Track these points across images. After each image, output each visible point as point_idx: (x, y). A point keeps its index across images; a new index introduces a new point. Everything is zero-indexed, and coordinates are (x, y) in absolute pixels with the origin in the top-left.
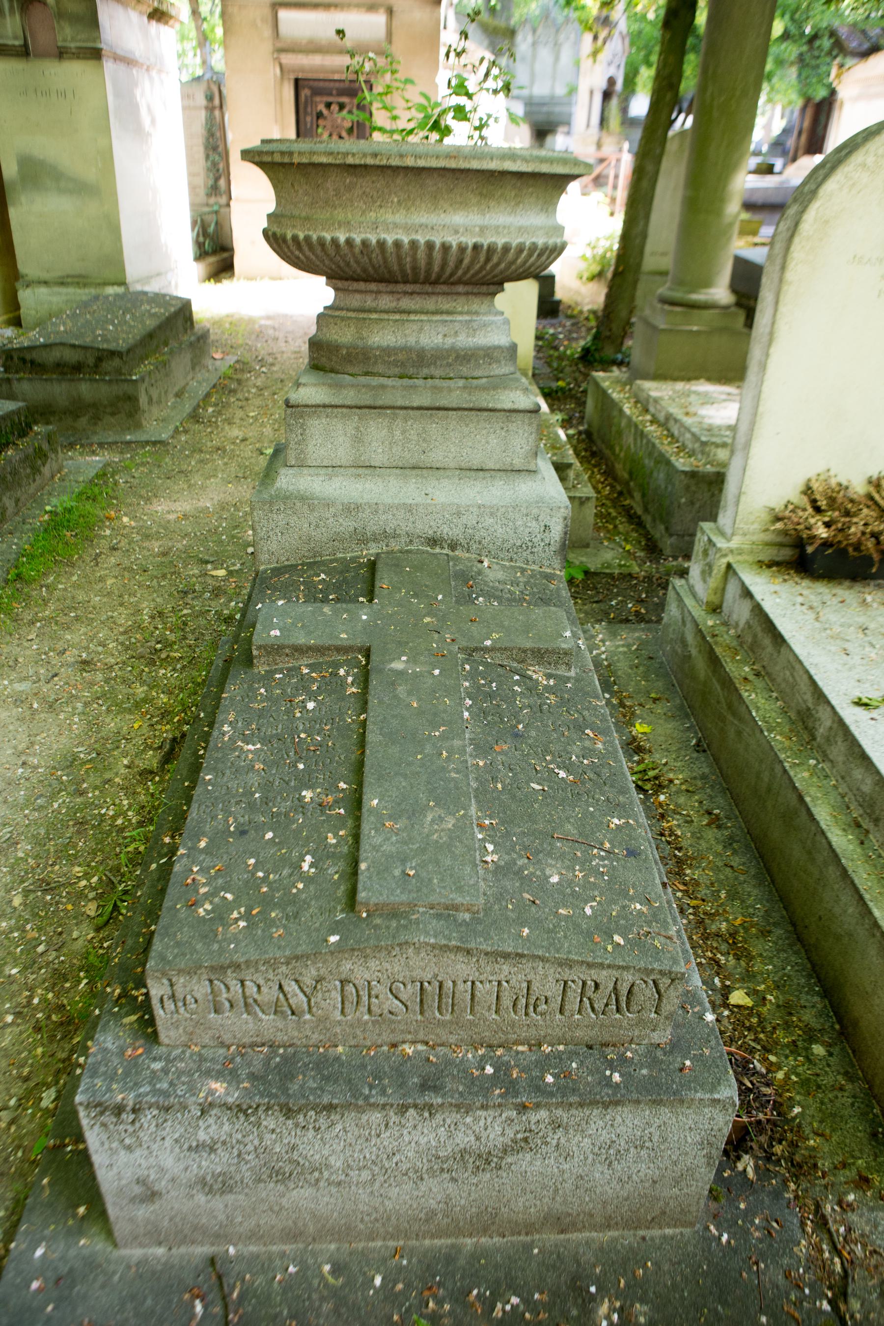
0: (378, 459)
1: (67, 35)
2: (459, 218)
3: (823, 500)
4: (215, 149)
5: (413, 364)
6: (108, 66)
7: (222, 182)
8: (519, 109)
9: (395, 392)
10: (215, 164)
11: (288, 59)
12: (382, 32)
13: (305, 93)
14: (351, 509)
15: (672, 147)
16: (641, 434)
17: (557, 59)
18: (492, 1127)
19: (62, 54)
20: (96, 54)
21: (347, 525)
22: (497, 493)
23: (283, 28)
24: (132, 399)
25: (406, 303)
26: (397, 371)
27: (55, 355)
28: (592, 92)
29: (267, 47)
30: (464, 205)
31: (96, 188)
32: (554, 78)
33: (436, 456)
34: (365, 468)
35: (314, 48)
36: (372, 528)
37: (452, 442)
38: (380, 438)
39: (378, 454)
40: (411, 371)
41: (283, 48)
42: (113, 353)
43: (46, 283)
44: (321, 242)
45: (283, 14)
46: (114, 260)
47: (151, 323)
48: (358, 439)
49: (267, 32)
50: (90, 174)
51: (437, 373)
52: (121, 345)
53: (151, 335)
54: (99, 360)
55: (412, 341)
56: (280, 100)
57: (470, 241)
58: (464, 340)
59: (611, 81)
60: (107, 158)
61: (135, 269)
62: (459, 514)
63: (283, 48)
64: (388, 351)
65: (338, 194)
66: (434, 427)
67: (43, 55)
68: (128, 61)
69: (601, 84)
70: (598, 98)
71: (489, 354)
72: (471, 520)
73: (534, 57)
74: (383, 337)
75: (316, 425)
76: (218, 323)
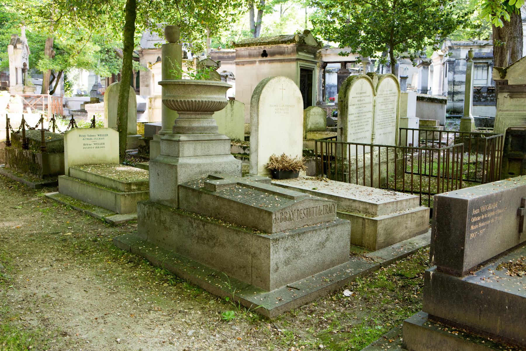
0: (199, 154)
2: (209, 96)
14: (199, 165)
16: (10, 221)
18: (323, 235)
21: (198, 170)
25: (198, 116)
26: (199, 132)
28: (16, 69)
30: (215, 93)
33: (211, 152)
36: (203, 170)
40: (203, 132)
44: (188, 101)
51: (208, 132)
55: (201, 125)
57: (218, 101)
59: (25, 65)
62: (221, 165)
64: (197, 127)
65: (191, 91)
66: (210, 144)
69: (21, 66)
70: (20, 72)
72: (223, 166)
74: (195, 124)
75: (186, 146)
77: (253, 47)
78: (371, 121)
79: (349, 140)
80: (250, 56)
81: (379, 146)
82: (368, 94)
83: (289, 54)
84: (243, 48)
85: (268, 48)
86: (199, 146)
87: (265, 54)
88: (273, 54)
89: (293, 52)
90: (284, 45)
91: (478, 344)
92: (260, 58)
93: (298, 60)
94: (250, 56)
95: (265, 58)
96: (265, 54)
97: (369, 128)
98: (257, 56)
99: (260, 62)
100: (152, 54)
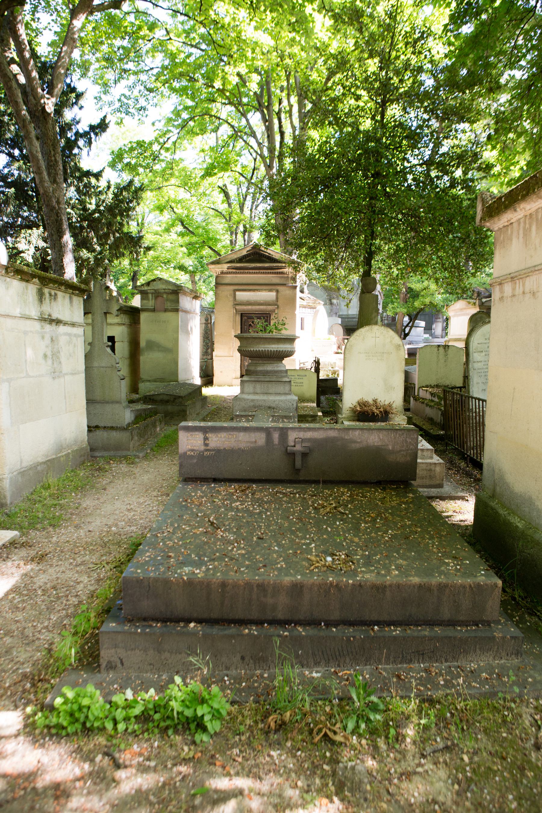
1: (169, 305)
2: (273, 346)
3: (363, 404)
4: (207, 338)
5: (266, 373)
6: (180, 313)
8: (339, 321)
9: (262, 378)
10: (207, 344)
11: (238, 307)
12: (274, 298)
13: (245, 318)
14: (253, 400)
19: (166, 310)
20: (177, 310)
21: (252, 404)
23: (237, 298)
24: (184, 411)
27: (161, 397)
29: (231, 303)
31: (172, 351)
33: (270, 391)
34: (255, 393)
35: (249, 303)
37: (273, 388)
38: (259, 387)
39: (258, 391)
41: (237, 303)
42: (180, 397)
43: (149, 381)
45: (238, 293)
46: (175, 373)
47: (190, 391)
48: (254, 388)
49: (232, 299)
50: (170, 345)
52: (182, 394)
53: (190, 394)
56: (235, 321)
58: (276, 369)
60: (176, 341)
61: (181, 377)
63: (237, 303)
66: (270, 385)
67: (160, 311)
68: (186, 312)
71: (281, 371)
74: (260, 368)
76: (210, 397)
86: (258, 386)
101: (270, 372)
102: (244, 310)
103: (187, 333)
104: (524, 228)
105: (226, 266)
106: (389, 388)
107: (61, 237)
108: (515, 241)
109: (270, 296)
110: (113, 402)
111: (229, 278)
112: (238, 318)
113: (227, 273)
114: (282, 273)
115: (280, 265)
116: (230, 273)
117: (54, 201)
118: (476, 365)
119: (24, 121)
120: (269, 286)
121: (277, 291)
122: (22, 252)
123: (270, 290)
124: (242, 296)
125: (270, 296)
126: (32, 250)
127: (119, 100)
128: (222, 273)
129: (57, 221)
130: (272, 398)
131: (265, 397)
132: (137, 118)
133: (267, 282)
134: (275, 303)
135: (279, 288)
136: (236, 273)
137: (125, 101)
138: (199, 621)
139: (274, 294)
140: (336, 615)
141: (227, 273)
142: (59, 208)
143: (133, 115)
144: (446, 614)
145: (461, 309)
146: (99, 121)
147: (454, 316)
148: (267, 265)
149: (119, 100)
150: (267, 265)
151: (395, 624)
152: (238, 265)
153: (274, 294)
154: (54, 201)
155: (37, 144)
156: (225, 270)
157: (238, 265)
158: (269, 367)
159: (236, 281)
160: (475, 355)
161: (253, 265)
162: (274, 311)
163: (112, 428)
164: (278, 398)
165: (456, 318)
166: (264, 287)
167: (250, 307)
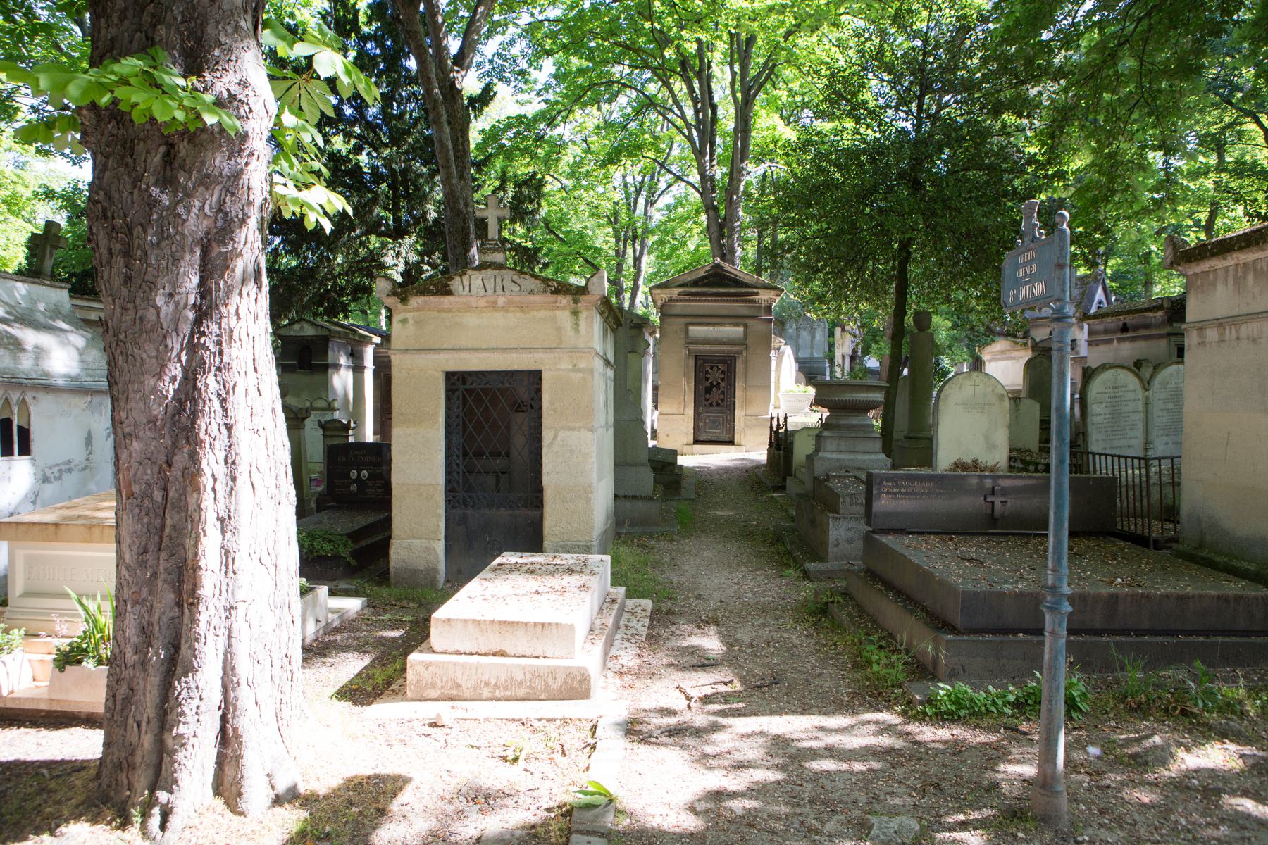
5: (851, 427)
7: (180, 459)
11: (692, 347)
12: (741, 335)
14: (838, 460)
15: (901, 383)
17: (813, 337)
22: (873, 457)
23: (691, 334)
29: (682, 342)
32: (812, 348)
34: (840, 452)
35: (706, 341)
38: (844, 445)
39: (843, 448)
45: (691, 328)
49: (683, 336)
54: (663, 467)
56: (686, 366)
63: (690, 342)
73: (798, 336)
74: (843, 422)
75: (828, 441)
77: (1109, 319)
78: (1140, 426)
79: (1094, 448)
80: (1106, 332)
81: (1159, 459)
82: (1131, 387)
83: (1158, 326)
84: (1096, 321)
85: (1129, 319)
86: (843, 442)
87: (1125, 329)
88: (1136, 328)
89: (1163, 323)
90: (1151, 314)
91: (1180, 717)
92: (1119, 335)
93: (1169, 335)
94: (1106, 332)
95: (1125, 335)
96: (1125, 329)
97: (1139, 432)
98: (1114, 332)
99: (1119, 340)
100: (1042, 326)
101: (857, 426)
102: (700, 351)
103: (646, 382)
104: (1235, 277)
105: (676, 291)
106: (991, 446)
107: (467, 250)
108: (1220, 288)
109: (736, 331)
110: (636, 465)
111: (679, 307)
112: (691, 362)
113: (677, 301)
114: (753, 301)
115: (743, 290)
116: (681, 300)
117: (461, 202)
118: (1095, 419)
119: (436, 101)
120: (734, 319)
121: (746, 326)
122: (388, 268)
123: (736, 325)
124: (697, 331)
125: (736, 331)
126: (401, 267)
127: (491, 61)
128: (671, 300)
129: (463, 229)
130: (860, 457)
131: (852, 457)
132: (513, 84)
133: (731, 313)
134: (742, 342)
135: (747, 321)
136: (689, 301)
137: (500, 62)
138: (1026, 632)
139: (741, 329)
140: (1146, 625)
141: (677, 301)
142: (467, 212)
143: (508, 81)
144: (1242, 624)
145: (1003, 352)
146: (479, 92)
147: (990, 361)
148: (732, 290)
149: (491, 61)
150: (732, 290)
151: (1198, 633)
152: (694, 290)
153: (741, 329)
154: (461, 202)
155: (447, 129)
156: (675, 296)
157: (694, 290)
158: (855, 420)
159: (689, 311)
160: (1094, 406)
161: (714, 290)
162: (741, 352)
163: (635, 497)
164: (867, 457)
165: (993, 364)
166: (728, 320)
167: (708, 347)
